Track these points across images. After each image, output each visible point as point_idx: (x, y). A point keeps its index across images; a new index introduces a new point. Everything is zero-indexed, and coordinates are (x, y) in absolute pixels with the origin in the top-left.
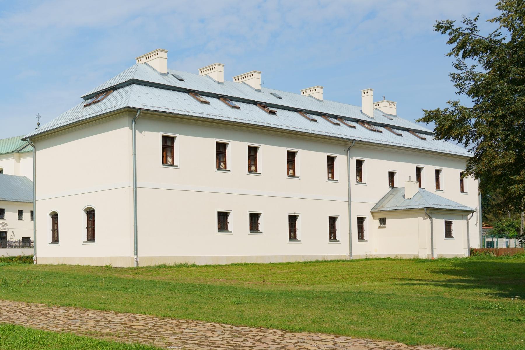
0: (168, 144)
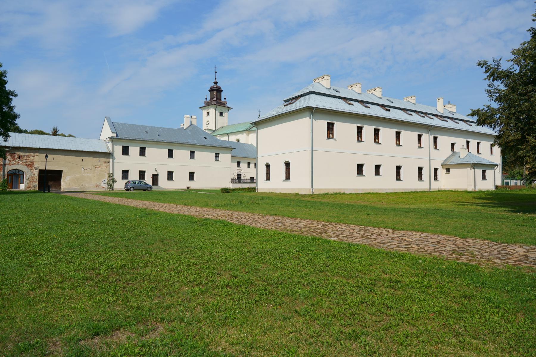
0: (330, 127)
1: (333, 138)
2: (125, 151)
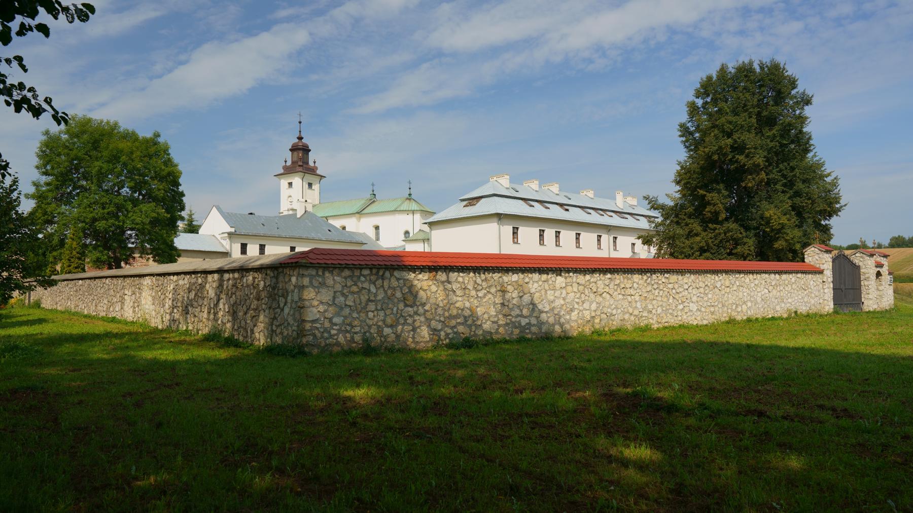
0: (515, 232)
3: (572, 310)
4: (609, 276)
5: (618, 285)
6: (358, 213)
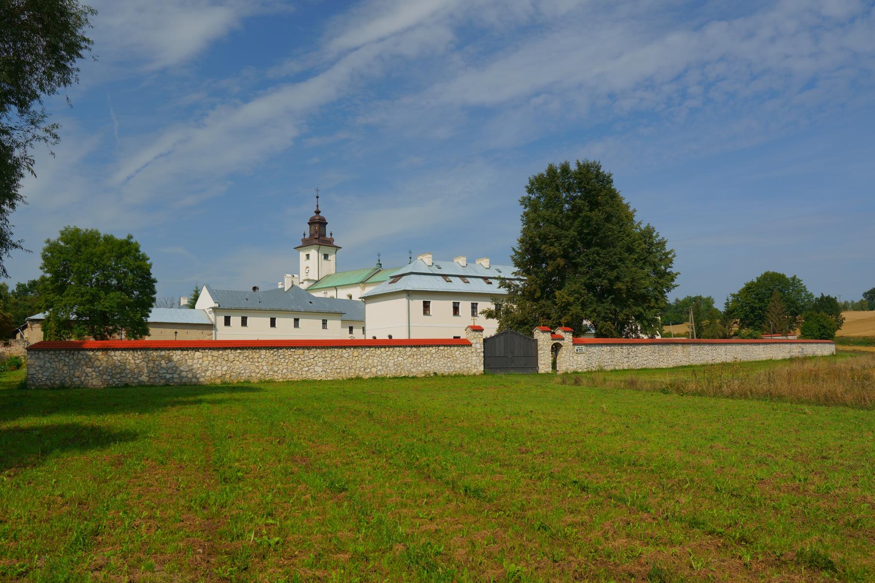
0: (426, 306)
1: (429, 315)
2: (227, 322)
3: (207, 370)
4: (239, 351)
5: (247, 357)
6: (362, 282)
